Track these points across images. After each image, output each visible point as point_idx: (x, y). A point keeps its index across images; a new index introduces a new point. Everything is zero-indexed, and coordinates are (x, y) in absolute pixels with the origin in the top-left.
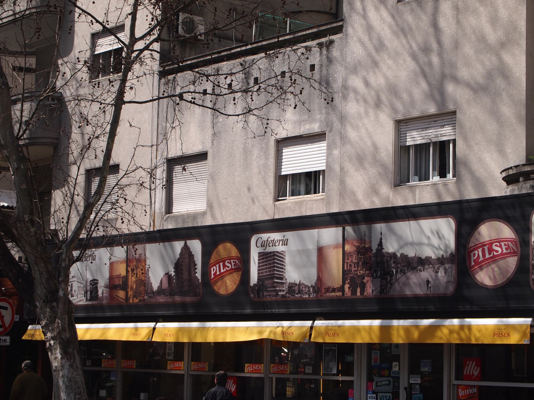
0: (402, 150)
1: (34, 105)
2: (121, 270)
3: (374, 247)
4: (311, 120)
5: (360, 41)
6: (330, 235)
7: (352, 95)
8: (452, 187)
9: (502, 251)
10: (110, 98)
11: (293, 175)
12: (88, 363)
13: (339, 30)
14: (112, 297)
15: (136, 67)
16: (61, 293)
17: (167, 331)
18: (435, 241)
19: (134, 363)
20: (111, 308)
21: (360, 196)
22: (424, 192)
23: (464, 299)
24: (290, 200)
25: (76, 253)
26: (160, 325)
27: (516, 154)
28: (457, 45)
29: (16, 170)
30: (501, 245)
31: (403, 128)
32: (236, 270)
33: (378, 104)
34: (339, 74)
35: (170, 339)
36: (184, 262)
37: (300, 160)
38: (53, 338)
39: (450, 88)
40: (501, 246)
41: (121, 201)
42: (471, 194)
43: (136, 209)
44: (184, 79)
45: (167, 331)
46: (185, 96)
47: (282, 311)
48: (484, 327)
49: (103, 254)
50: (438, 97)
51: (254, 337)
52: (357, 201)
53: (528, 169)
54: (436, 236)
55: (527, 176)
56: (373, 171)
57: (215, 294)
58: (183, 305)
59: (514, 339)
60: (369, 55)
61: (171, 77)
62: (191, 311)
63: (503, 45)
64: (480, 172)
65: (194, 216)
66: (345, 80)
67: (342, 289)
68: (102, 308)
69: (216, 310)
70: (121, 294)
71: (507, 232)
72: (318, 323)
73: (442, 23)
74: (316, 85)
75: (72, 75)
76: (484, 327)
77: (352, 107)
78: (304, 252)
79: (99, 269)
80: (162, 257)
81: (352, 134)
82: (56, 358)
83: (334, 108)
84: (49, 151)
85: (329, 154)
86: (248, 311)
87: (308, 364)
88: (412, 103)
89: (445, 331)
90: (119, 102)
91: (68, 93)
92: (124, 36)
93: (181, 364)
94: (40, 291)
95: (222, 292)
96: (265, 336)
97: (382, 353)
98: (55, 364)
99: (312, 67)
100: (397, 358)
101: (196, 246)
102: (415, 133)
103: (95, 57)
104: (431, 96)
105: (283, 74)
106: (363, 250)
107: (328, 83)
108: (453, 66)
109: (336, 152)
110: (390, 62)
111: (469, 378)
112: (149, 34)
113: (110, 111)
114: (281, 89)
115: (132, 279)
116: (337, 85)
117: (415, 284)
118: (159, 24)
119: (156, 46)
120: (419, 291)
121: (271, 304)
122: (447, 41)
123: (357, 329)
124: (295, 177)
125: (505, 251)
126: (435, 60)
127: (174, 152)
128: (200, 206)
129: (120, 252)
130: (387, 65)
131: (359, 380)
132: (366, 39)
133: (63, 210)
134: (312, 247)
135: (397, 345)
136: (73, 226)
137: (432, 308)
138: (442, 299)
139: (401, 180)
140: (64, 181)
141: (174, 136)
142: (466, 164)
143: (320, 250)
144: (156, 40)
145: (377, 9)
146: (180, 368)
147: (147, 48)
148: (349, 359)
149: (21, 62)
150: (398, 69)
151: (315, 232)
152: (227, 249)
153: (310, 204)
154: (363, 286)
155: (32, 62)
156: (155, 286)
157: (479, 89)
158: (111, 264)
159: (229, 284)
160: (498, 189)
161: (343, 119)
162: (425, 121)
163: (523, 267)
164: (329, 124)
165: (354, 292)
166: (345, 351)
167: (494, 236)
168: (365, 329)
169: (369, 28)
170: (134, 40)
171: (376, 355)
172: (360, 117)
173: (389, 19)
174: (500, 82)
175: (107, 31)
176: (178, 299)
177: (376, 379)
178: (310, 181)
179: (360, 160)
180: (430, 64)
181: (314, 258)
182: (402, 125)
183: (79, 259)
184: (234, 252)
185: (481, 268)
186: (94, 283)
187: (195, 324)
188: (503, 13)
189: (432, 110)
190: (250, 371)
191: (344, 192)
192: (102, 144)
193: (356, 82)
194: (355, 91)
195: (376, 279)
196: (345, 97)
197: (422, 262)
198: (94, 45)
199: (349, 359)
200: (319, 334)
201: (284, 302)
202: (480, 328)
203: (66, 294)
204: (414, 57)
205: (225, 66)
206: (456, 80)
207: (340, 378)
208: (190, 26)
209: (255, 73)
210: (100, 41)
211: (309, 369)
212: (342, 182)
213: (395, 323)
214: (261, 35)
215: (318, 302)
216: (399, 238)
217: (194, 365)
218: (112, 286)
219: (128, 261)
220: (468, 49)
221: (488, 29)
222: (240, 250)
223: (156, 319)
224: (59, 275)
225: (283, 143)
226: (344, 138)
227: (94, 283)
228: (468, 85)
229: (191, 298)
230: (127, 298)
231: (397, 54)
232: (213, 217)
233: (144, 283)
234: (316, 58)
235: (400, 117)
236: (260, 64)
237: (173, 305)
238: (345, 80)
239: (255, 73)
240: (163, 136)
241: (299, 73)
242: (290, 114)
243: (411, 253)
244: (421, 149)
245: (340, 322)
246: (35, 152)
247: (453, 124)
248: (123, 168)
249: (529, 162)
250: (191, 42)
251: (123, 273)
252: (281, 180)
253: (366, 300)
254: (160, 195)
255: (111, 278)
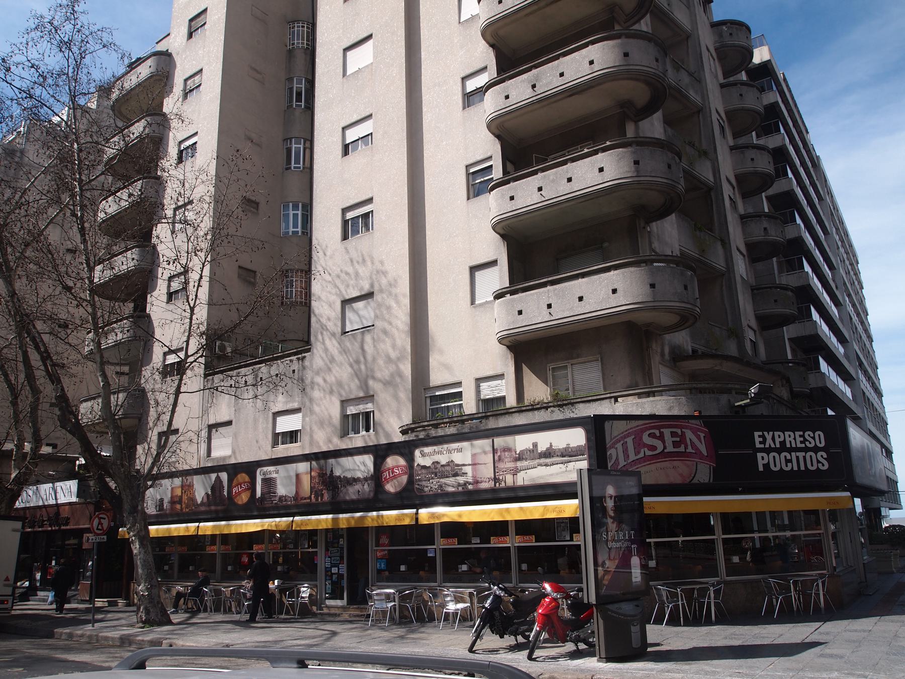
0: (344, 417)
1: (125, 394)
2: (178, 492)
3: (328, 473)
4: (294, 401)
5: (322, 358)
6: (303, 467)
7: (316, 387)
8: (373, 437)
9: (665, 448)
10: (172, 390)
11: (283, 433)
12: (158, 549)
13: (309, 350)
14: (172, 508)
15: (188, 372)
16: (140, 508)
17: (207, 527)
18: (362, 468)
19: (186, 548)
20: (171, 515)
21: (321, 444)
22: (358, 440)
23: (379, 499)
24: (281, 447)
25: (149, 483)
26: (202, 524)
27: (407, 418)
28: (374, 359)
29: (113, 434)
30: (662, 434)
31: (345, 405)
32: (248, 489)
33: (331, 392)
34: (309, 375)
35: (209, 533)
36: (217, 486)
37: (286, 424)
38: (134, 536)
39: (371, 382)
40: (661, 438)
41: (178, 451)
42: (383, 441)
43: (189, 455)
44: (217, 378)
45: (207, 527)
46: (220, 389)
47: (275, 512)
48: (391, 516)
49: (166, 482)
50: (364, 387)
51: (259, 529)
52: (320, 447)
53: (413, 426)
54: (363, 465)
55: (413, 430)
56: (329, 430)
57: (236, 504)
58: (216, 512)
59: (407, 522)
60: (326, 364)
61: (210, 378)
62: (221, 515)
63: (398, 359)
64: (388, 429)
65: (224, 458)
66: (312, 378)
67: (310, 498)
68: (166, 515)
69: (236, 514)
70: (178, 506)
71: (402, 461)
72: (297, 518)
73: (366, 347)
74: (295, 382)
75: (150, 377)
76: (391, 516)
77: (316, 394)
78: (289, 477)
79: (165, 493)
80: (204, 483)
81: (316, 409)
82: (136, 548)
83: (306, 394)
84: (135, 422)
85: (303, 420)
86: (255, 513)
87: (291, 543)
88: (351, 391)
89: (370, 520)
90: (178, 392)
91: (148, 387)
92: (182, 355)
93: (215, 547)
94: (126, 506)
95: (240, 503)
96: (265, 528)
97: (333, 534)
98: (135, 552)
99: (294, 371)
100: (342, 536)
101: (224, 476)
102: (352, 408)
103: (165, 366)
104: (361, 388)
105: (277, 375)
106: (322, 475)
107: (302, 380)
108: (372, 370)
109: (307, 419)
110: (337, 368)
111: (383, 545)
112: (196, 353)
113: (172, 397)
114: (275, 384)
115: (185, 498)
116: (308, 381)
117: (352, 493)
118: (202, 347)
119: (202, 360)
120: (354, 497)
121: (269, 509)
122: (369, 358)
123: (319, 521)
124: (284, 434)
125: (670, 448)
126: (363, 367)
127: (212, 422)
128: (227, 452)
129: (177, 481)
130: (336, 370)
131: (321, 550)
132: (324, 355)
133: (143, 458)
134: (293, 474)
135: (342, 529)
136: (147, 467)
137: (361, 506)
138: (367, 501)
139: (344, 434)
140: (145, 439)
141: (211, 411)
142: (381, 425)
143: (297, 476)
144: (201, 356)
145: (330, 339)
146: (214, 549)
147: (195, 361)
148: (315, 538)
149: (118, 369)
150: (343, 372)
151: (294, 465)
152: (243, 477)
153: (293, 449)
154: (322, 495)
155: (126, 369)
156: (199, 501)
157: (387, 383)
158: (172, 489)
159: (244, 498)
160: (398, 438)
161: (311, 400)
162: (358, 400)
163: (411, 481)
164: (303, 403)
165: (317, 500)
166: (313, 534)
167: (395, 464)
168: (324, 520)
169: (326, 350)
170: (187, 356)
171: (330, 535)
172: (321, 399)
173: (337, 344)
174: (398, 380)
175: (171, 352)
176: (213, 508)
177: (330, 549)
178: (292, 436)
179: (321, 424)
180: (360, 370)
181: (294, 481)
182: (344, 403)
183: (151, 486)
184: (247, 478)
185: (388, 482)
186: (162, 500)
187: (223, 523)
188: (399, 342)
189: (361, 394)
190: (256, 549)
191: (312, 442)
192: (166, 418)
193: (319, 380)
194: (318, 385)
195: (330, 491)
196: (312, 388)
197: (356, 480)
198: (165, 360)
199: (315, 538)
200: (297, 525)
201: (277, 507)
202: (388, 517)
203: (143, 508)
204: (351, 366)
205: (243, 371)
206: (373, 378)
207: (311, 550)
208: (223, 348)
209: (260, 375)
210: (168, 357)
211: (291, 546)
212: (311, 436)
213: (341, 516)
214: (264, 352)
215: (296, 506)
216: (342, 467)
217: (223, 547)
218: (173, 502)
219: (182, 487)
220: (381, 362)
221: (390, 351)
222: (250, 478)
223: (199, 521)
224: (139, 496)
225: (276, 414)
226: (312, 412)
227: (162, 500)
228: (380, 381)
229: (221, 506)
230: (182, 509)
231: (341, 363)
232: (236, 458)
233: (192, 499)
234: (296, 366)
235: (344, 399)
236: (264, 369)
237: (210, 512)
238: (312, 378)
239: (260, 375)
240: (205, 412)
241: (285, 375)
242: (281, 398)
243: (349, 475)
244: (355, 416)
245: (309, 517)
246: (126, 423)
247: (373, 402)
248: (180, 431)
249: (414, 422)
250: (223, 357)
251: (180, 494)
252: (276, 436)
253: (324, 504)
254: (203, 447)
255: (172, 497)
